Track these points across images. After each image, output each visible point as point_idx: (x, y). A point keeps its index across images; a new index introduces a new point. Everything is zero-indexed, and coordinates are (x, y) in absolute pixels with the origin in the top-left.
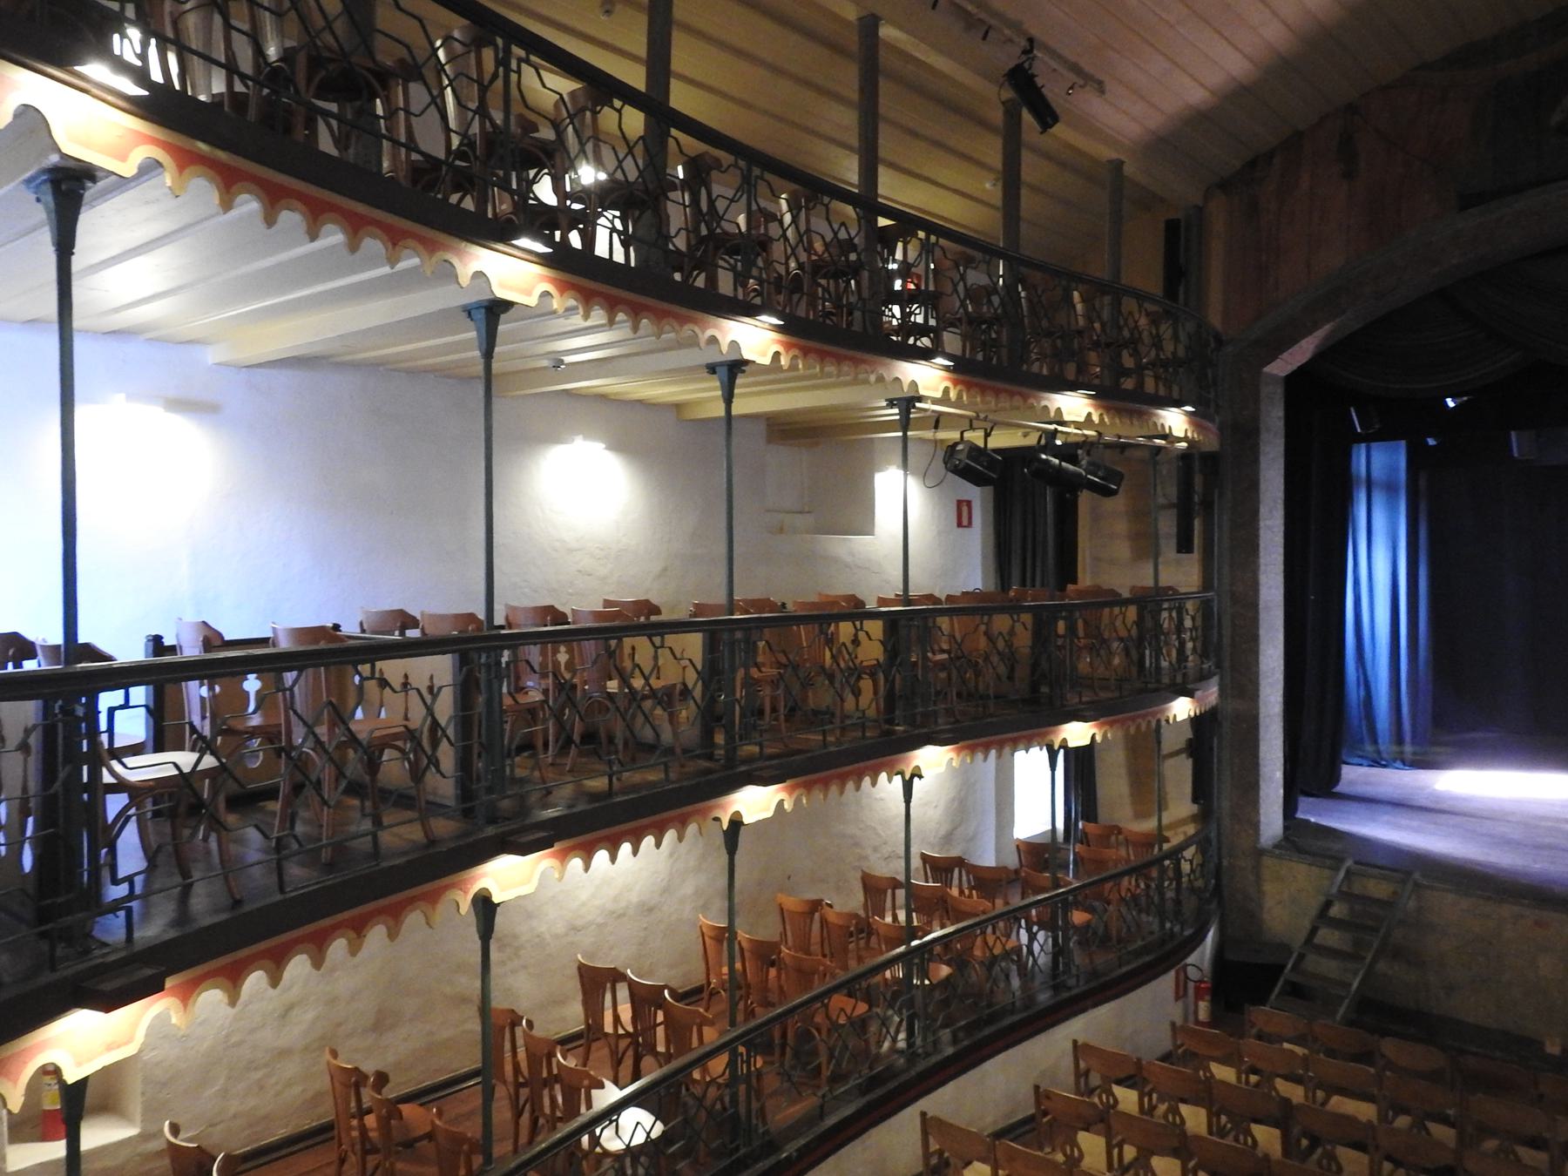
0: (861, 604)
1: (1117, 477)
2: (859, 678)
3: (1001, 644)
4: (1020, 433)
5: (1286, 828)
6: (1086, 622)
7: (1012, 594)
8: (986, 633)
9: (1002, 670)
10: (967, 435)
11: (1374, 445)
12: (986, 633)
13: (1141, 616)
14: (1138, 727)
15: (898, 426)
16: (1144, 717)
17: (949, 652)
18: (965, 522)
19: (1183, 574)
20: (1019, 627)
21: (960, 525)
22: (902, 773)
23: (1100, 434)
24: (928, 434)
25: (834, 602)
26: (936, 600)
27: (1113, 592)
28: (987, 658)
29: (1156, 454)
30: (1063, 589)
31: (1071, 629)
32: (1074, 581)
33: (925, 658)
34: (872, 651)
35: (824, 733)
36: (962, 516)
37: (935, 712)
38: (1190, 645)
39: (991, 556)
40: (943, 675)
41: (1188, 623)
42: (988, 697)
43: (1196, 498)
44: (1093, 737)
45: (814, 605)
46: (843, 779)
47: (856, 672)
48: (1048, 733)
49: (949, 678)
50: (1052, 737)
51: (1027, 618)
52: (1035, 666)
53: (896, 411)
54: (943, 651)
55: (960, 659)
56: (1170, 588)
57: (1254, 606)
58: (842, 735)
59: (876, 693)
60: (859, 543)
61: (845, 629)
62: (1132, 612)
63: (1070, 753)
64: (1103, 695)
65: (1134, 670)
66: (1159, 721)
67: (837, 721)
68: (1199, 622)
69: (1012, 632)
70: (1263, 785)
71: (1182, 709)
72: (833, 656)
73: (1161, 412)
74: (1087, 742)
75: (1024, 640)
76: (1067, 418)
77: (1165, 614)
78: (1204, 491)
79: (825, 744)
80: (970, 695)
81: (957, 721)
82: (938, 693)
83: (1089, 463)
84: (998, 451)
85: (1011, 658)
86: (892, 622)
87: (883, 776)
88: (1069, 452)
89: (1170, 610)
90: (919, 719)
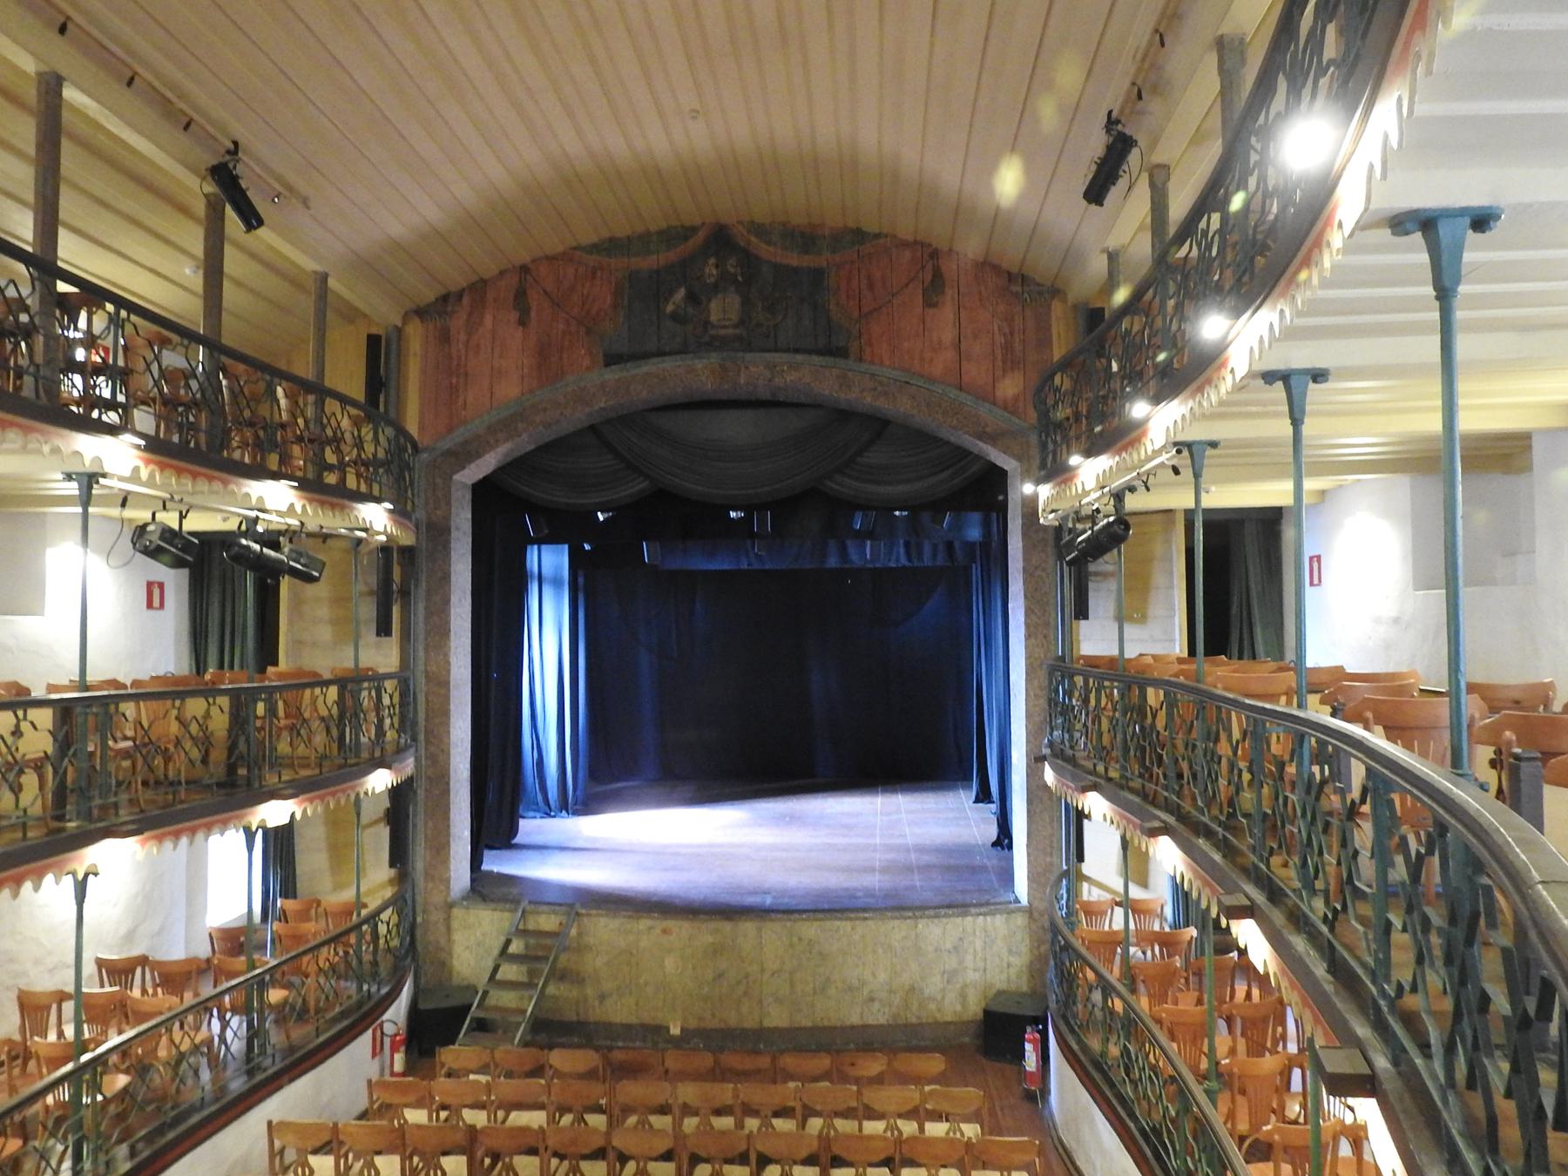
0: (27, 691)
2: (21, 772)
3: (194, 728)
4: (219, 517)
5: (473, 880)
7: (208, 677)
9: (195, 754)
13: (341, 695)
14: (338, 802)
17: (134, 739)
18: (156, 603)
19: (383, 656)
20: (215, 711)
22: (74, 874)
27: (315, 674)
28: (178, 742)
30: (262, 670)
31: (272, 711)
32: (276, 664)
36: (154, 595)
38: (388, 721)
40: (126, 764)
41: (386, 701)
49: (134, 765)
51: (224, 701)
52: (232, 748)
53: (74, 485)
54: (125, 738)
55: (146, 746)
59: (42, 787)
60: (25, 625)
62: (333, 692)
64: (304, 773)
65: (335, 746)
66: (358, 794)
68: (396, 699)
69: (207, 715)
71: (380, 781)
73: (360, 506)
74: (287, 821)
75: (220, 722)
77: (365, 693)
80: (158, 783)
84: (190, 533)
85: (205, 742)
86: (65, 711)
90: (95, 812)
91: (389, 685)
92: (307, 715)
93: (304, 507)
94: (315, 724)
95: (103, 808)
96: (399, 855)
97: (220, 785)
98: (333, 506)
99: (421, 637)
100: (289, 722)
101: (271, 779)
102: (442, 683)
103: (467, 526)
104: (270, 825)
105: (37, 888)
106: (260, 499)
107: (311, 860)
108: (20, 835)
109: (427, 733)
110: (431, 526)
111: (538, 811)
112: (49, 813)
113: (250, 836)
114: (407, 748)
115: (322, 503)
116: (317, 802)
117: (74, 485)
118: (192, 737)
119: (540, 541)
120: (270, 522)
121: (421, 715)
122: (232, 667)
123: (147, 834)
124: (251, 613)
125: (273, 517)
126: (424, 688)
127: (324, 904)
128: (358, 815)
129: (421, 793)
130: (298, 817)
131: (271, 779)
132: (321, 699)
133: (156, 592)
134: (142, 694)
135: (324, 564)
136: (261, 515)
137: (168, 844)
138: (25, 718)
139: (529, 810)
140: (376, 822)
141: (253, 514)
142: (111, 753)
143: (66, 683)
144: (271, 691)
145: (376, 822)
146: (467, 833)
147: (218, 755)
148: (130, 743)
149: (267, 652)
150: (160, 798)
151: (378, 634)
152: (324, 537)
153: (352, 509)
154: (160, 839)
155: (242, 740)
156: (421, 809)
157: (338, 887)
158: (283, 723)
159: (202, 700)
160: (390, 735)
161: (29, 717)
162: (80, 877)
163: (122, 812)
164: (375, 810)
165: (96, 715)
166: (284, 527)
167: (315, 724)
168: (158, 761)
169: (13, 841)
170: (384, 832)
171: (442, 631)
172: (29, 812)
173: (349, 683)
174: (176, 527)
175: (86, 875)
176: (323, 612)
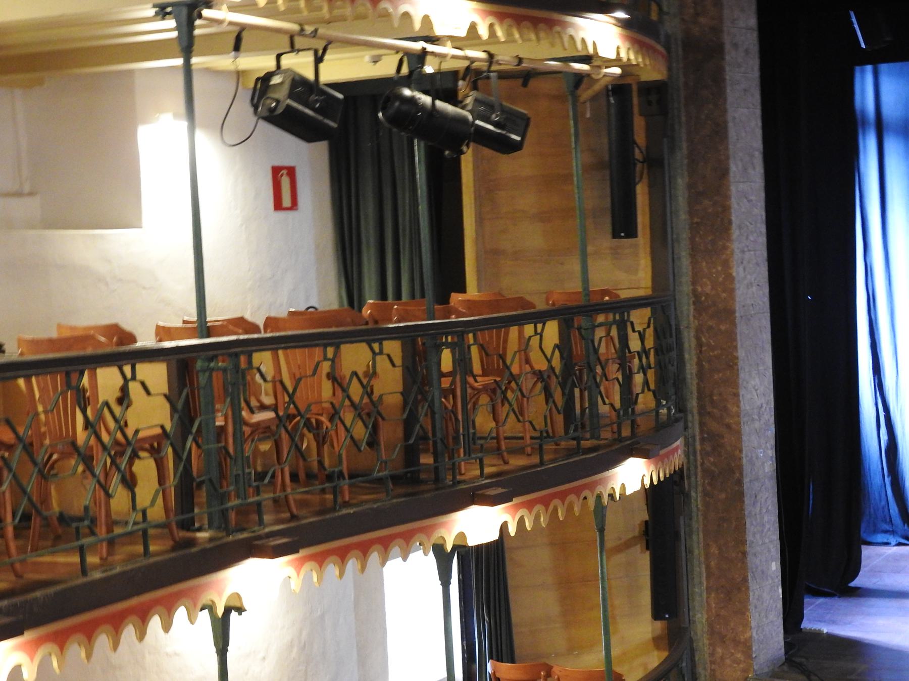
0: (131, 338)
1: (521, 123)
2: (135, 456)
3: (356, 391)
4: (367, 55)
5: (788, 645)
6: (482, 347)
7: (366, 312)
8: (329, 376)
9: (360, 431)
10: (288, 61)
11: (884, 67)
12: (332, 377)
13: (564, 335)
14: (570, 509)
15: (177, 48)
16: (577, 491)
17: (275, 408)
18: (287, 201)
19: (627, 272)
20: (382, 363)
21: (278, 206)
22: (211, 608)
23: (491, 56)
24: (225, 62)
25: (85, 338)
26: (252, 327)
27: (522, 302)
28: (334, 415)
29: (573, 82)
30: (443, 299)
31: (462, 363)
32: (462, 289)
33: (239, 421)
34: (151, 414)
35: (82, 551)
36: (282, 187)
37: (259, 504)
38: (638, 379)
39: (338, 260)
40: (265, 447)
41: (635, 344)
42: (341, 475)
43: (638, 154)
44: (504, 528)
45: (51, 343)
46: (116, 624)
47: (127, 449)
48: (433, 528)
49: (277, 445)
50: (442, 532)
51: (393, 347)
52: (409, 424)
53: (171, 23)
54: (263, 407)
55: (292, 420)
56: (605, 292)
57: (728, 314)
58: (110, 552)
59: (161, 479)
60: (117, 240)
61: (108, 380)
62: (552, 330)
63: (461, 549)
64: (517, 462)
65: (559, 419)
66: (599, 497)
67: (102, 531)
68: (650, 343)
69: (372, 374)
70: (753, 585)
71: (632, 475)
72: (87, 424)
73: (577, 20)
74: (494, 536)
75: (390, 382)
76: (438, 31)
77: (600, 333)
78: (637, 142)
79: (84, 569)
80: (310, 476)
81: (293, 517)
82: (261, 476)
83: (477, 101)
84: (335, 86)
85: (371, 413)
86: (182, 364)
87: (181, 613)
88: (445, 86)
89: (608, 325)
90: (232, 516)
91: (640, 317)
92: (515, 369)
93: (491, 26)
94: (527, 383)
95: (242, 511)
96: (667, 600)
97: (395, 479)
98: (535, 23)
99: (685, 235)
100: (489, 380)
101: (470, 471)
102: (720, 313)
103: (751, 41)
104: (472, 542)
105: (167, 627)
106: (426, 20)
107: (533, 602)
108: (140, 548)
109: (700, 398)
110: (690, 44)
111: (893, 533)
112: (173, 519)
113: (443, 558)
114: (671, 422)
115: (519, 20)
116: (539, 508)
117: (171, 23)
118: (353, 404)
119: (877, 57)
120: (444, 57)
121: (691, 368)
122: (398, 296)
123: (303, 552)
124: (423, 208)
125: (447, 49)
126: (694, 323)
127: (556, 670)
128: (602, 530)
129: (697, 499)
130: (512, 530)
131: (470, 471)
132: (535, 341)
133: (285, 182)
134: (284, 337)
135: (527, 120)
136: (430, 48)
137: (332, 569)
138: (134, 377)
139: (876, 531)
140: (627, 545)
141: (418, 46)
142: (247, 430)
143: (179, 324)
144: (460, 330)
145: (627, 545)
146: (775, 566)
147: (391, 432)
148: (270, 415)
149: (450, 277)
150: (315, 499)
151: (615, 235)
152: (524, 76)
153: (564, 25)
154: (320, 560)
155: (423, 410)
156: (698, 524)
157: (574, 648)
158: (482, 381)
159: (364, 346)
160: (646, 401)
161: (140, 376)
162: (220, 612)
163: (267, 518)
164: (626, 525)
165: (225, 370)
166: (462, 65)
167: (527, 383)
168: (308, 442)
169: (132, 557)
170: (643, 561)
171: (715, 225)
172: (150, 514)
173: (575, 315)
174: (310, 75)
175: (228, 611)
176: (528, 200)
